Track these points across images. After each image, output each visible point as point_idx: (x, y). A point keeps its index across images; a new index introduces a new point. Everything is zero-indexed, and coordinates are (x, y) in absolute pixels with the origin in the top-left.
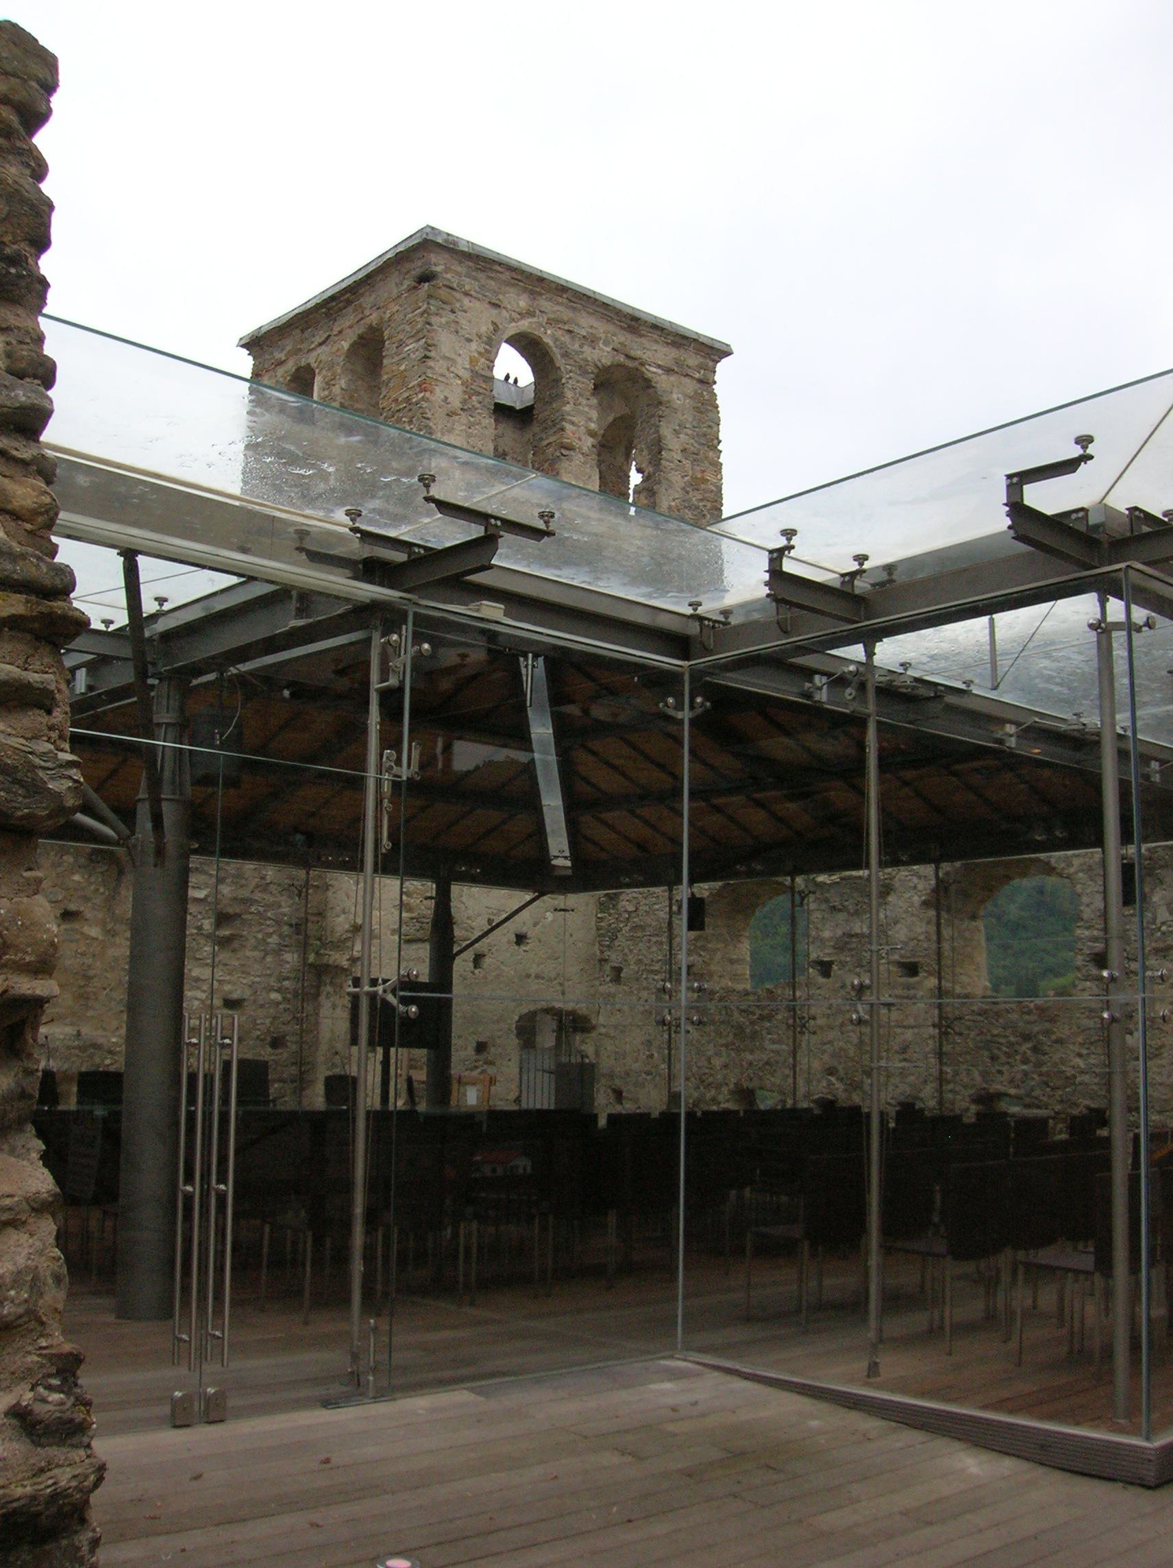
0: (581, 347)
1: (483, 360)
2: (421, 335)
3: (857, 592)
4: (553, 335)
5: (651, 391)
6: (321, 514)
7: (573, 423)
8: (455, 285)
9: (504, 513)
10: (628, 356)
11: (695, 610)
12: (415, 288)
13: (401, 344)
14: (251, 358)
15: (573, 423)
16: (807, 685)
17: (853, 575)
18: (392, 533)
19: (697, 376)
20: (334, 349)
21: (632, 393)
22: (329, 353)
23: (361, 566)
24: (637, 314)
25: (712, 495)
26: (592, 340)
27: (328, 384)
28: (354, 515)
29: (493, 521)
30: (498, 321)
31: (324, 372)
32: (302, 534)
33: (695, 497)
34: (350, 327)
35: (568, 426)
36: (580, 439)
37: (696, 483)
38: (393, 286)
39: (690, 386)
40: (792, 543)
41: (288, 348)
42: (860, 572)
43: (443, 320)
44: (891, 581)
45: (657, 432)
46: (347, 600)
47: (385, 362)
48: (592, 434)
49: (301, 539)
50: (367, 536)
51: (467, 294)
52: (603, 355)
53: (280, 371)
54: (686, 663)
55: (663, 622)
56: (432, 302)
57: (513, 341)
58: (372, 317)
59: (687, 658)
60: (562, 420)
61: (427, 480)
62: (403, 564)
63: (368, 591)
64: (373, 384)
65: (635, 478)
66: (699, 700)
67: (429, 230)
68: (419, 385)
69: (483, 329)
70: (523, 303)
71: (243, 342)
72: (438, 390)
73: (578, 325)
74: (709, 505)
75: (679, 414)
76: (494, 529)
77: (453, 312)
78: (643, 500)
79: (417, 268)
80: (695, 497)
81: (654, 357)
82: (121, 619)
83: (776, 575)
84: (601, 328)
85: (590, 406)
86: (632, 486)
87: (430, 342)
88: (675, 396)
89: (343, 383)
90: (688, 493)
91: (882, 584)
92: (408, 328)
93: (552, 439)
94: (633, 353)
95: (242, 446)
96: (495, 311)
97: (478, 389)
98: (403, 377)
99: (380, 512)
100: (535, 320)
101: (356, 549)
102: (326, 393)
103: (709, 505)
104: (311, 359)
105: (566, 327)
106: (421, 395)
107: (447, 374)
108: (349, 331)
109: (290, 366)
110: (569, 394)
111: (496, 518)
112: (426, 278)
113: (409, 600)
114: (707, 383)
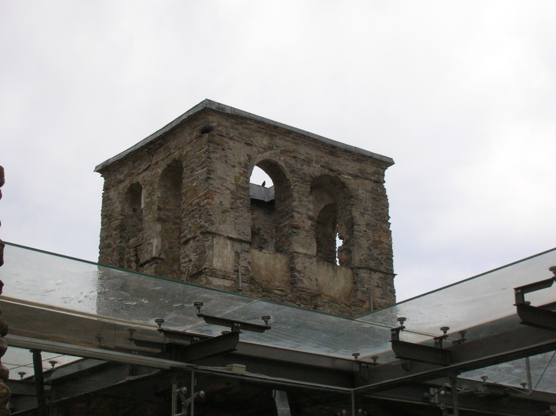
0: (302, 166)
1: (242, 178)
2: (205, 165)
3: (444, 347)
4: (285, 160)
5: (345, 189)
6: (142, 322)
7: (299, 213)
8: (224, 134)
9: (242, 319)
10: (331, 170)
11: (356, 358)
12: (200, 136)
13: (193, 170)
14: (103, 178)
15: (299, 213)
16: (426, 394)
17: (441, 338)
18: (180, 329)
19: (373, 178)
20: (153, 173)
21: (332, 196)
22: (150, 175)
23: (165, 346)
24: (334, 144)
25: (386, 251)
26: (308, 162)
27: (150, 195)
28: (160, 322)
29: (236, 325)
30: (251, 154)
31: (147, 187)
32: (132, 331)
33: (375, 252)
34: (163, 160)
35: (296, 215)
36: (303, 222)
37: (376, 244)
38: (187, 136)
39: (369, 185)
40: (404, 325)
41: (126, 172)
42: (445, 337)
43: (218, 155)
44: (463, 340)
45: (351, 214)
46: (157, 368)
47: (184, 181)
48: (310, 218)
49: (131, 334)
50: (168, 333)
51: (231, 138)
52: (315, 170)
53: (121, 186)
54: (352, 389)
55: (338, 364)
56: (211, 144)
57: (260, 165)
58: (176, 154)
59: (354, 387)
60: (293, 211)
61: (198, 305)
62: (189, 346)
63: (168, 363)
64: (177, 193)
65: (339, 243)
66: (360, 411)
67: (207, 102)
68: (205, 195)
69: (242, 159)
70: (265, 142)
71: (98, 169)
72: (216, 197)
73: (299, 153)
74: (384, 257)
75: (363, 203)
76: (237, 327)
77: (223, 150)
78: (344, 256)
79: (201, 124)
80: (375, 252)
81: (346, 168)
82: (30, 372)
83: (397, 343)
84: (313, 153)
85: (309, 201)
86: (337, 246)
87: (210, 169)
88: (360, 192)
89: (159, 194)
90: (371, 250)
91: (459, 342)
92: (197, 160)
93: (287, 223)
94: (333, 168)
95: (96, 293)
96: (249, 148)
97: (240, 195)
98: (195, 190)
99: (175, 319)
100: (273, 151)
101: (161, 339)
102: (149, 200)
103: (384, 257)
104: (140, 179)
105: (292, 155)
106: (206, 201)
107: (222, 188)
108: (162, 162)
109: (127, 183)
110: (295, 195)
111: (237, 322)
112: (207, 130)
113: (192, 367)
114: (380, 182)
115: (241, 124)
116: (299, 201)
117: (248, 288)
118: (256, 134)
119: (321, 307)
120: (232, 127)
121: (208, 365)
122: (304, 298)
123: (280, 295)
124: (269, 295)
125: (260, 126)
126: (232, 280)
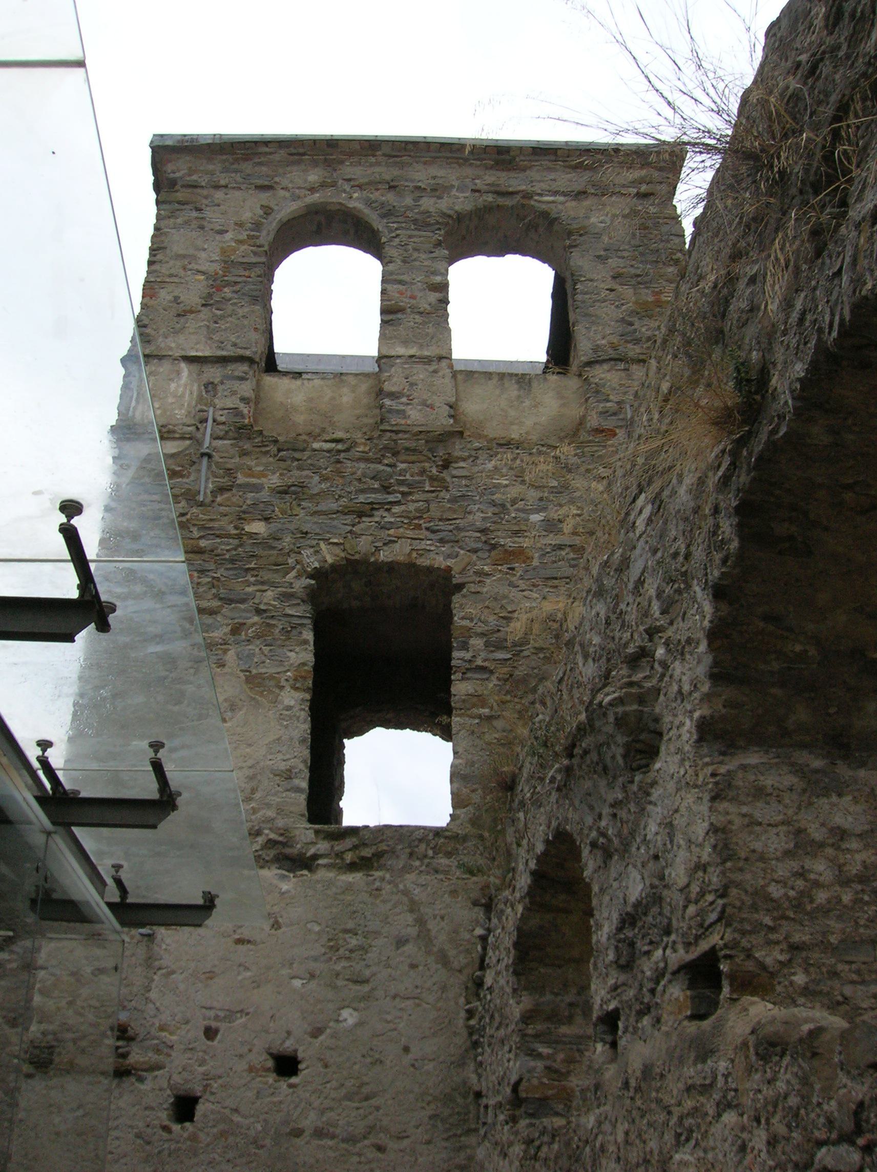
26: (437, 190)
115: (246, 158)
116: (404, 262)
117: (234, 451)
118: (289, 169)
119: (464, 460)
120: (225, 170)
121: (586, 932)
122: (407, 449)
123: (329, 451)
124: (297, 455)
125: (294, 151)
126: (182, 438)
